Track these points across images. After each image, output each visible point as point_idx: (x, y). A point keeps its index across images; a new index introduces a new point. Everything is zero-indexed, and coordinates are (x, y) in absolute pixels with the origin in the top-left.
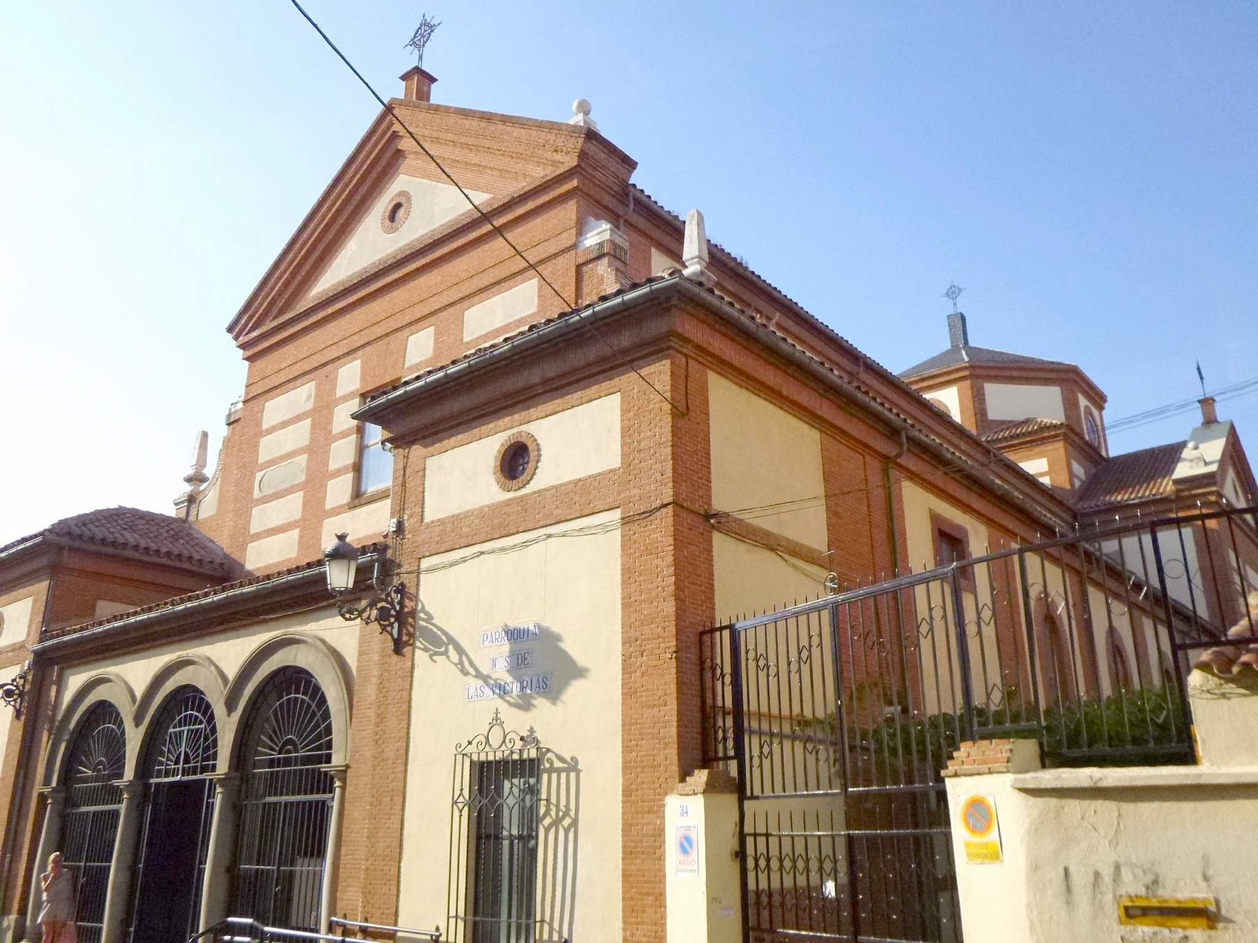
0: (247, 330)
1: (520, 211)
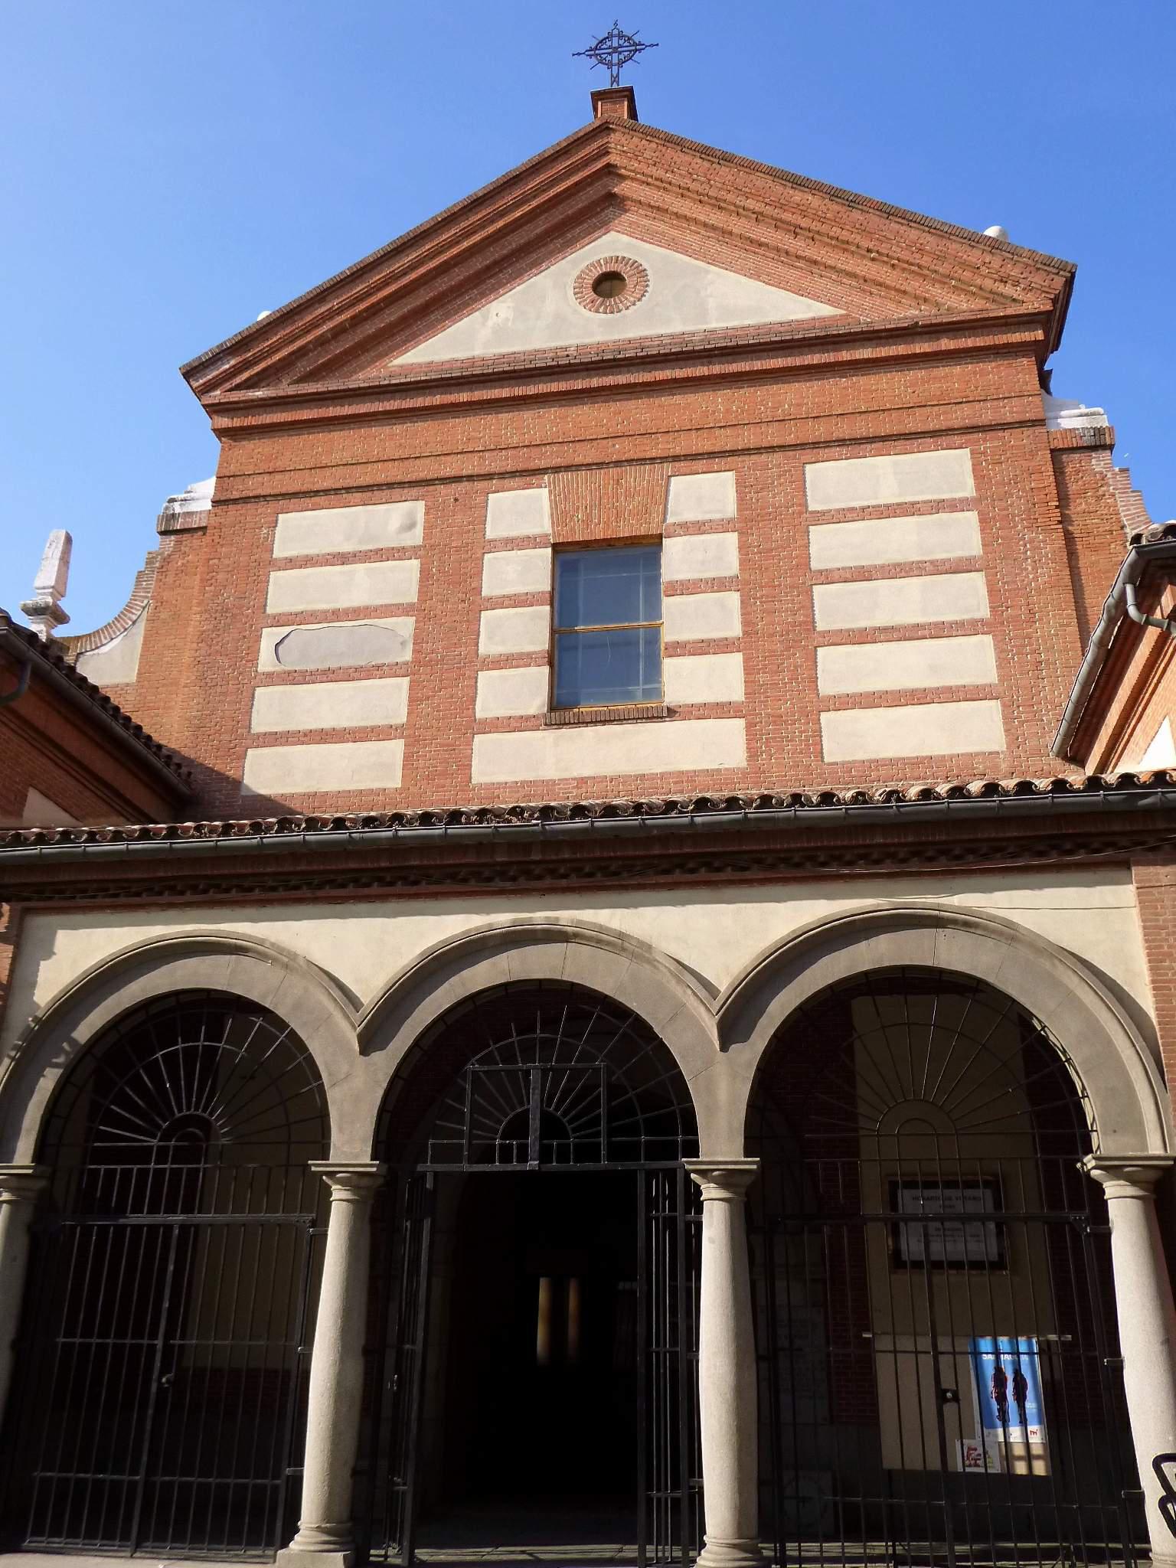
0: (238, 380)
1: (946, 344)
